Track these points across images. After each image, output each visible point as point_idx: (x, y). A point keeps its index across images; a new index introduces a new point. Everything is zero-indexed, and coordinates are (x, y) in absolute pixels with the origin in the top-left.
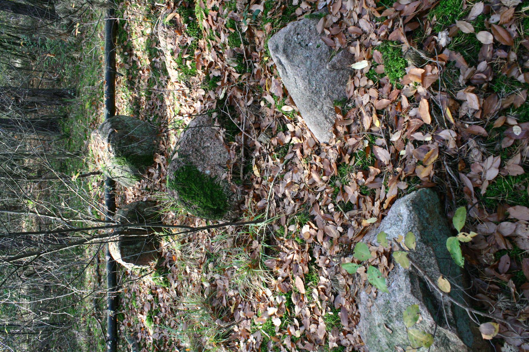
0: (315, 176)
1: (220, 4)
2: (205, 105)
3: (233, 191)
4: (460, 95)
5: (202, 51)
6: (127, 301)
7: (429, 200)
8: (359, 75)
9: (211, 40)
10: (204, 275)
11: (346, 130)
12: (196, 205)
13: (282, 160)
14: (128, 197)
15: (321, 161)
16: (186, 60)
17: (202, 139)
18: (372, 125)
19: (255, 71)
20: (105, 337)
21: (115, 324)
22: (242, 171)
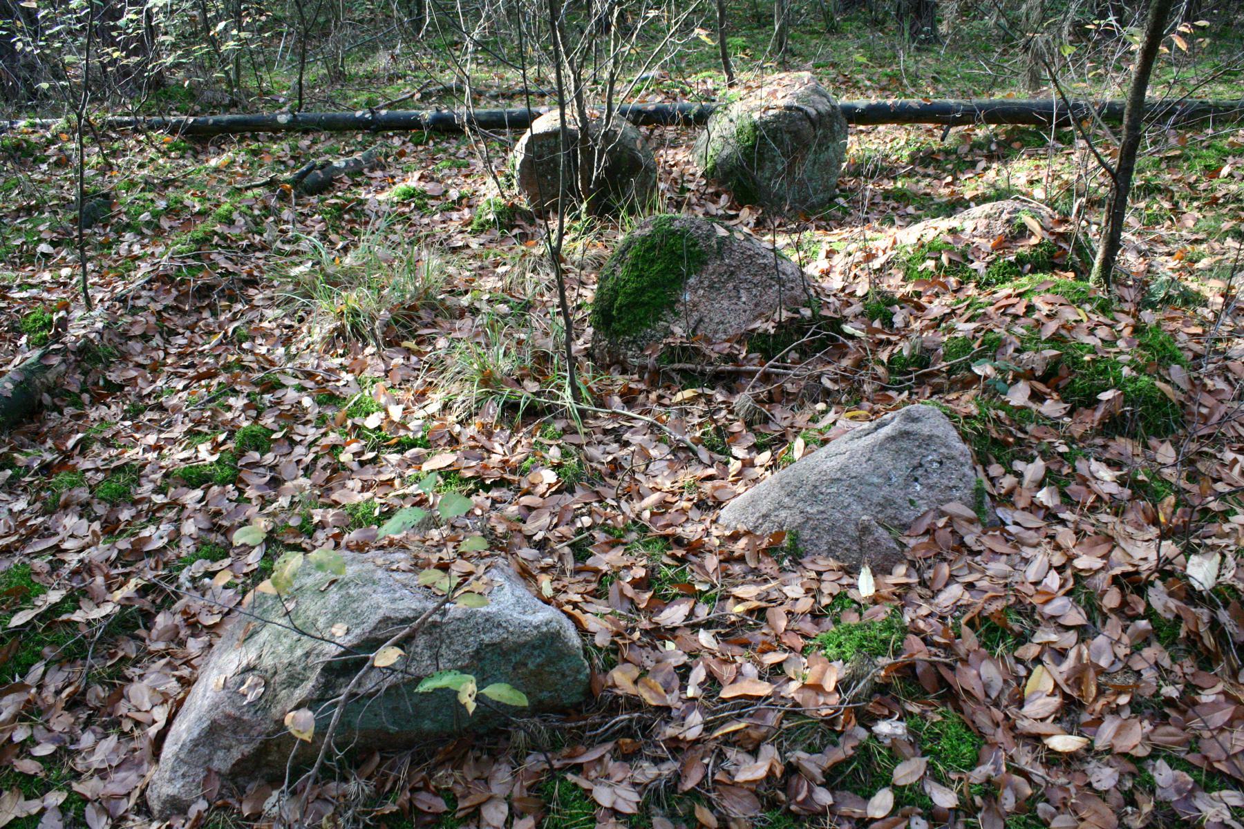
0: (654, 498)
1: (1037, 320)
2: (835, 295)
4: (769, 753)
5: (955, 291)
6: (452, 151)
7: (564, 676)
8: (846, 580)
9: (968, 306)
10: (486, 297)
11: (736, 554)
12: (621, 272)
13: (699, 441)
14: (671, 152)
15: (683, 511)
16: (937, 259)
17: (756, 285)
18: (739, 600)
19: (893, 394)
20: (382, 108)
21: (407, 126)
22: (688, 366)
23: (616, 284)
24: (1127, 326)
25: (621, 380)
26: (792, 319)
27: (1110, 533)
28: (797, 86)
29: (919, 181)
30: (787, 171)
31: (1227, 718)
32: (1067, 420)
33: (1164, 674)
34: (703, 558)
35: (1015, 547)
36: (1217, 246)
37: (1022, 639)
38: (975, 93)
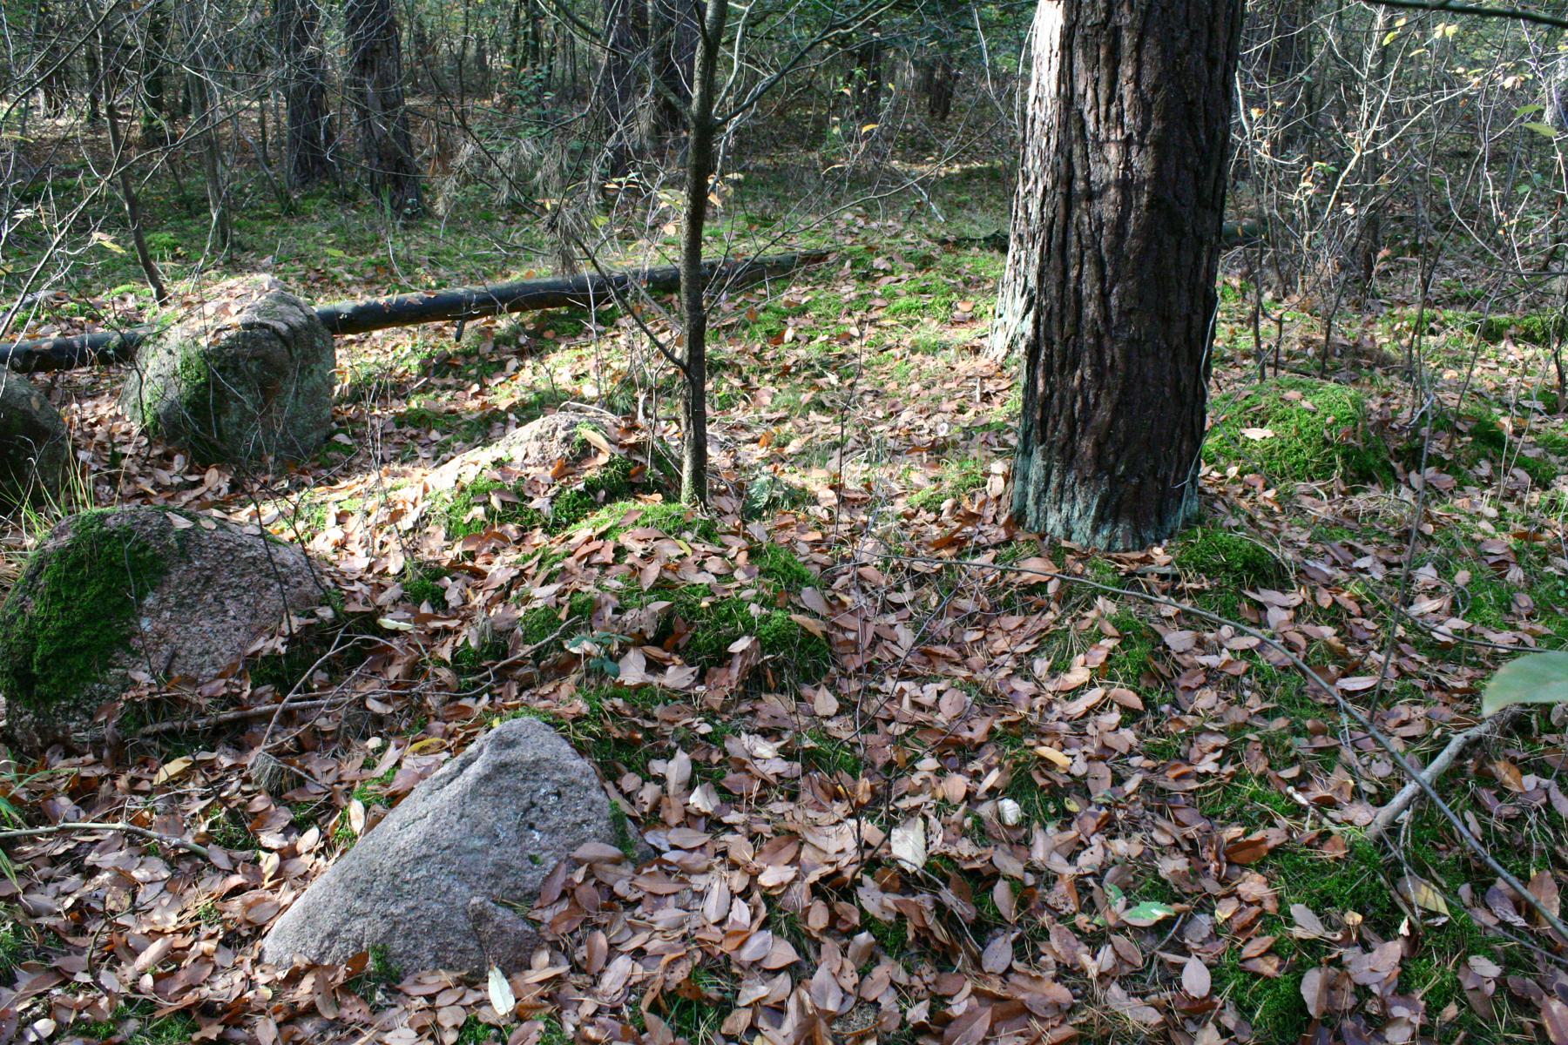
1: (632, 566)
2: (360, 579)
3: (99, 714)
5: (517, 542)
8: (472, 997)
9: (541, 562)
11: (302, 1005)
12: (34, 608)
13: (207, 839)
14: (88, 404)
15: (205, 957)
16: (486, 504)
17: (246, 590)
19: (467, 702)
22: (166, 726)
23: (30, 627)
24: (740, 550)
25: (63, 767)
26: (308, 626)
27: (792, 827)
28: (255, 295)
29: (437, 396)
30: (262, 412)
31: (987, 1027)
32: (700, 689)
33: (904, 993)
34: (253, 1027)
35: (682, 881)
36: (801, 422)
37: (725, 1007)
38: (486, 275)
